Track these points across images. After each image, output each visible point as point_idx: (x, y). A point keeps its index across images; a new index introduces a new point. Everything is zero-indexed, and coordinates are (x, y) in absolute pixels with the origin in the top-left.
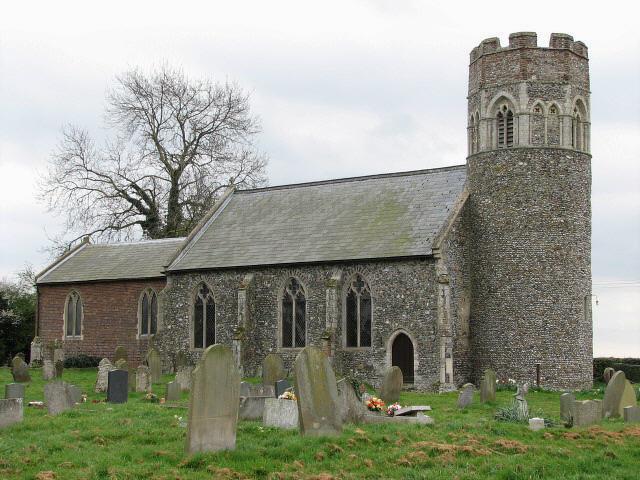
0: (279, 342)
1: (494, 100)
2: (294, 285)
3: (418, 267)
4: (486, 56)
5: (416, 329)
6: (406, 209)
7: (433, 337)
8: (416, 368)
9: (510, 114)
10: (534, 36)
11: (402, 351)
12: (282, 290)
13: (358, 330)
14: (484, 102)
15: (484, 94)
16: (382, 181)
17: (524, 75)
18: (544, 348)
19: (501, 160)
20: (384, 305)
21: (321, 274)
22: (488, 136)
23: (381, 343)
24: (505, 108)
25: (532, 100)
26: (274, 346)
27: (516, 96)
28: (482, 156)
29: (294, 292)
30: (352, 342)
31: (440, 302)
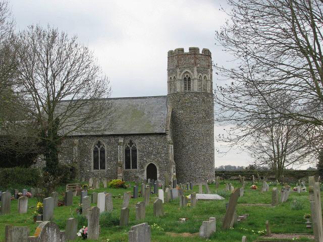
0: (92, 167)
1: (183, 72)
2: (99, 144)
3: (159, 137)
4: (171, 54)
5: (159, 162)
6: (144, 114)
7: (166, 165)
8: (158, 177)
9: (189, 78)
10: (182, 50)
11: (152, 172)
12: (93, 146)
13: (131, 160)
14: (179, 73)
15: (178, 70)
16: (126, 100)
17: (196, 64)
18: (204, 169)
19: (187, 97)
20: (143, 152)
21: (113, 140)
22: (179, 87)
23: (142, 167)
24: (187, 76)
25: (198, 74)
26: (90, 169)
27: (193, 72)
28: (178, 94)
29: (99, 147)
30: (128, 167)
31: (170, 151)
